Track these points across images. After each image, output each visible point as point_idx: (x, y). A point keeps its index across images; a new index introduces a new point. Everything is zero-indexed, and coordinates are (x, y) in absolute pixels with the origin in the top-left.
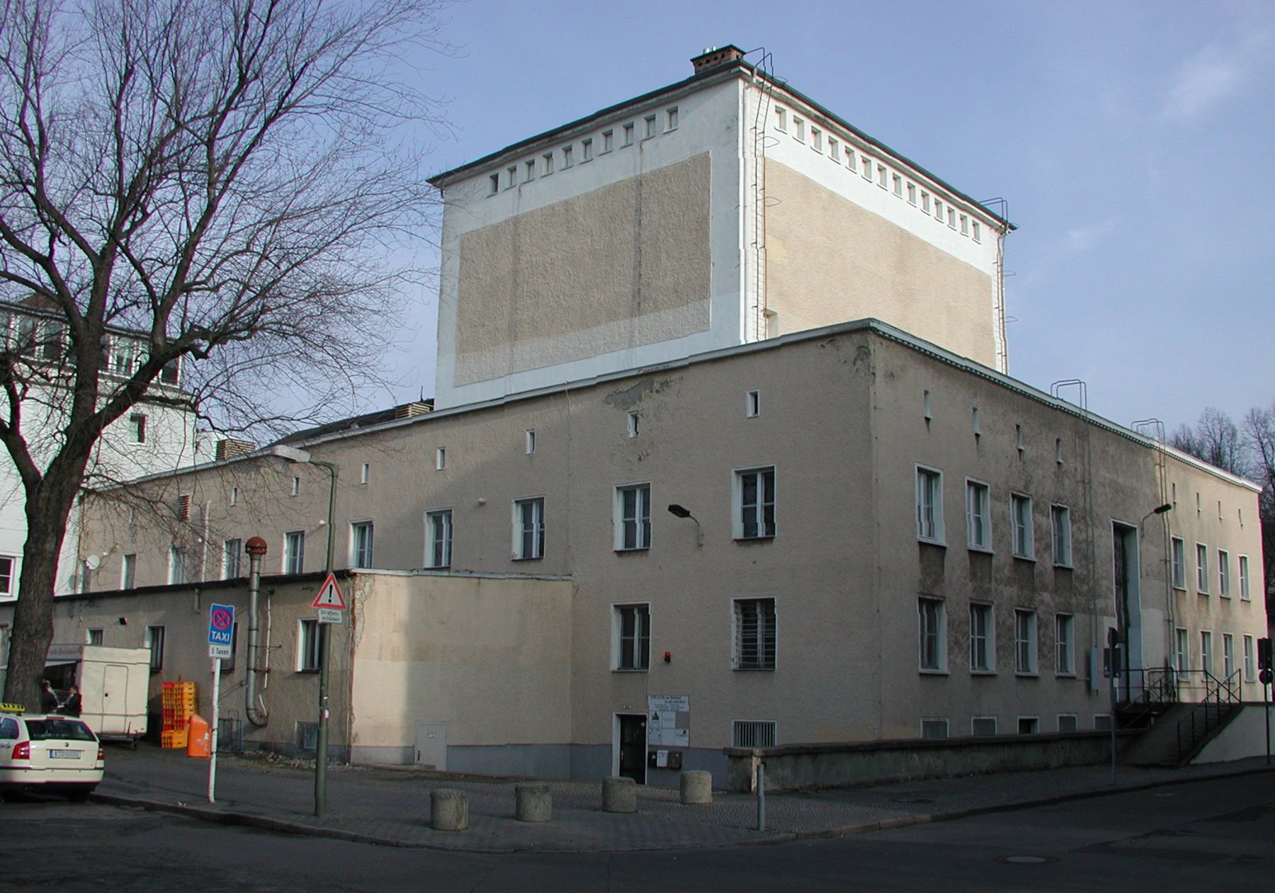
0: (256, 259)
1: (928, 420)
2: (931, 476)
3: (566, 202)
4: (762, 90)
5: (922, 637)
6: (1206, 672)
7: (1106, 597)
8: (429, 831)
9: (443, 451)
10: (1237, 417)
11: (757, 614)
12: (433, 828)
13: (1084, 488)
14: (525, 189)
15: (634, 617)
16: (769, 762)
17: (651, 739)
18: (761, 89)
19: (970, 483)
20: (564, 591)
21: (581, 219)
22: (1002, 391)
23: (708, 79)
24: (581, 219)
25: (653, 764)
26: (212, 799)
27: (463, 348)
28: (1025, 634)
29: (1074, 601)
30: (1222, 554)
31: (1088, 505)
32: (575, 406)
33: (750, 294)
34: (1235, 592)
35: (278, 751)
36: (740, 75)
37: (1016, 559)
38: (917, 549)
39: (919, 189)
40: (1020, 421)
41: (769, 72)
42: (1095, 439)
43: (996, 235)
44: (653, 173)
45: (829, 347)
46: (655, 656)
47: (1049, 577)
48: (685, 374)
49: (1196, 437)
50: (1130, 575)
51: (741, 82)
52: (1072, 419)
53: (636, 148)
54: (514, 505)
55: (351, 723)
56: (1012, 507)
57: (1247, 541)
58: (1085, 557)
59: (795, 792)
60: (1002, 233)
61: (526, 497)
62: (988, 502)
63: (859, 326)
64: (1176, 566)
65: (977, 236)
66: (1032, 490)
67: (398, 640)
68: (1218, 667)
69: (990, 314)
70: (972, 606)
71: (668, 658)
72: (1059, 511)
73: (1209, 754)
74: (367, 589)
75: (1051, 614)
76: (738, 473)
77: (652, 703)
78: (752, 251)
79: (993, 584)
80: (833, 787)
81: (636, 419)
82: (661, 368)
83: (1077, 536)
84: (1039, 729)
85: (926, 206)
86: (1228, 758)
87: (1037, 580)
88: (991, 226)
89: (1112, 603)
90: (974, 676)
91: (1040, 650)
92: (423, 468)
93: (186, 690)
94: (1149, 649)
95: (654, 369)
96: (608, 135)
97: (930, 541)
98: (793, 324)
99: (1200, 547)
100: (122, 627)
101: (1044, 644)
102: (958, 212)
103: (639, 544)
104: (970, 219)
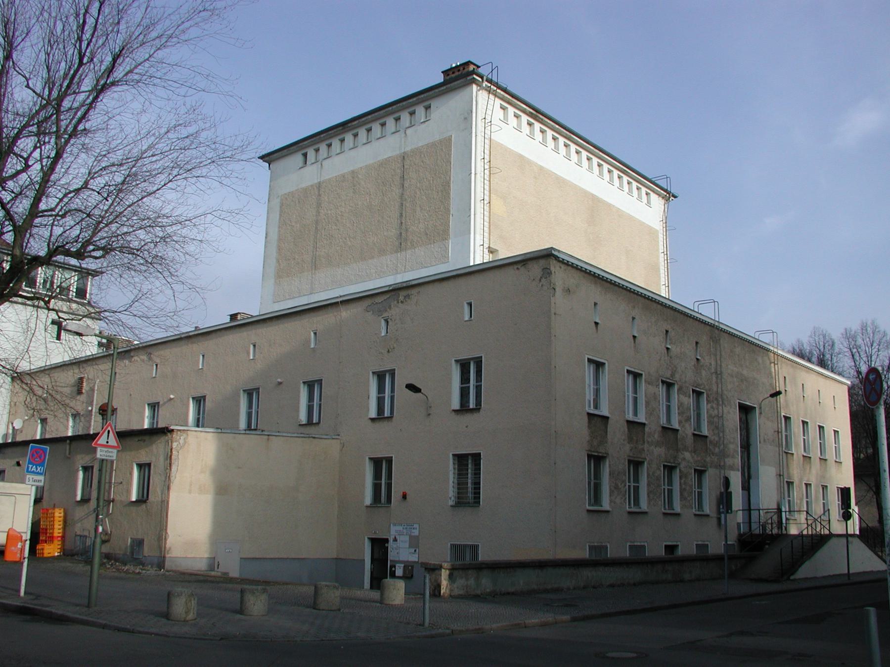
0: (101, 198)
1: (596, 324)
2: (598, 365)
3: (353, 172)
4: (489, 92)
5: (589, 483)
6: (807, 513)
7: (733, 457)
8: (164, 620)
9: (254, 346)
10: (836, 334)
11: (468, 463)
12: (168, 619)
13: (717, 378)
14: (325, 163)
15: (381, 466)
16: (456, 573)
17: (392, 556)
18: (490, 92)
19: (628, 372)
20: (333, 447)
21: (363, 183)
22: (655, 305)
23: (452, 85)
24: (363, 183)
25: (393, 575)
26: (22, 593)
27: (280, 275)
28: (670, 483)
29: (708, 459)
30: (821, 427)
31: (720, 390)
32: (345, 313)
33: (478, 236)
34: (830, 455)
35: (117, 560)
36: (474, 81)
37: (663, 428)
38: (586, 418)
39: (606, 167)
40: (669, 327)
41: (495, 79)
42: (725, 342)
43: (662, 201)
44: (412, 151)
45: (522, 269)
46: (396, 495)
47: (690, 440)
48: (421, 289)
49: (807, 348)
50: (752, 441)
51: (474, 86)
52: (708, 327)
53: (402, 133)
54: (302, 385)
55: (166, 539)
56: (662, 390)
57: (838, 419)
58: (717, 428)
59: (476, 598)
60: (667, 200)
61: (310, 378)
62: (643, 386)
63: (545, 253)
64: (786, 436)
65: (649, 202)
66: (677, 377)
67: (206, 479)
68: (817, 509)
69: (658, 257)
70: (630, 462)
71: (404, 496)
72: (698, 394)
73: (805, 571)
74: (182, 441)
75: (691, 468)
76: (457, 361)
77: (394, 530)
78: (479, 205)
79: (646, 445)
80: (508, 593)
81: (387, 322)
82: (405, 285)
83: (711, 412)
84: (680, 552)
85: (611, 179)
86: (819, 575)
87: (679, 443)
88: (659, 195)
89: (738, 461)
90: (629, 513)
91: (681, 494)
92: (249, 357)
93: (57, 514)
94: (767, 494)
95: (400, 286)
96: (383, 125)
97: (596, 412)
98: (505, 253)
99: (804, 423)
100: (18, 468)
101: (685, 489)
102: (635, 184)
103: (387, 413)
104: (644, 190)
